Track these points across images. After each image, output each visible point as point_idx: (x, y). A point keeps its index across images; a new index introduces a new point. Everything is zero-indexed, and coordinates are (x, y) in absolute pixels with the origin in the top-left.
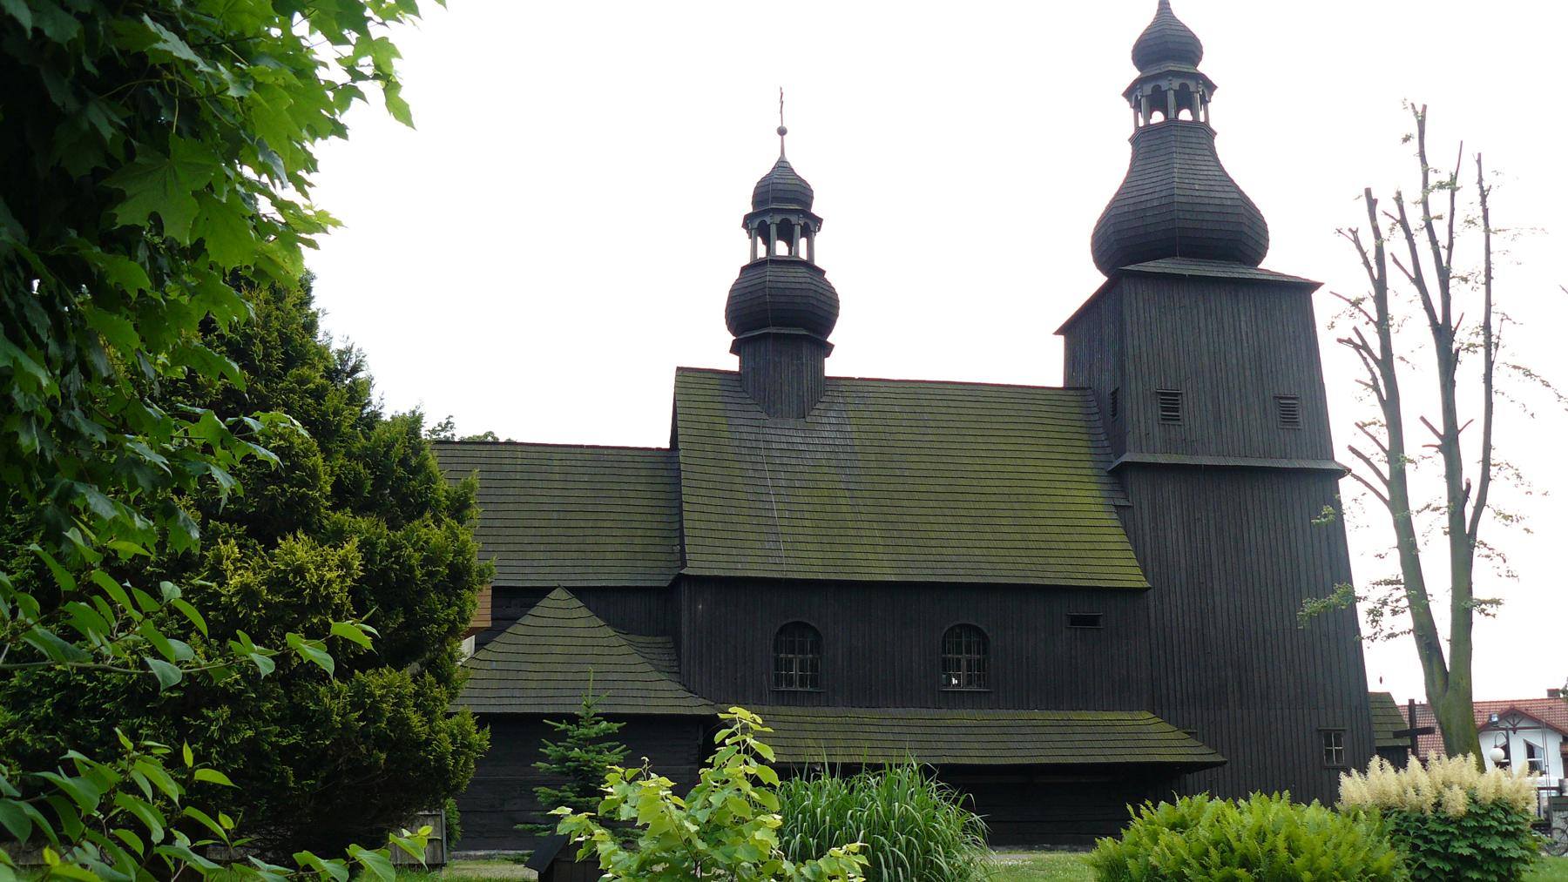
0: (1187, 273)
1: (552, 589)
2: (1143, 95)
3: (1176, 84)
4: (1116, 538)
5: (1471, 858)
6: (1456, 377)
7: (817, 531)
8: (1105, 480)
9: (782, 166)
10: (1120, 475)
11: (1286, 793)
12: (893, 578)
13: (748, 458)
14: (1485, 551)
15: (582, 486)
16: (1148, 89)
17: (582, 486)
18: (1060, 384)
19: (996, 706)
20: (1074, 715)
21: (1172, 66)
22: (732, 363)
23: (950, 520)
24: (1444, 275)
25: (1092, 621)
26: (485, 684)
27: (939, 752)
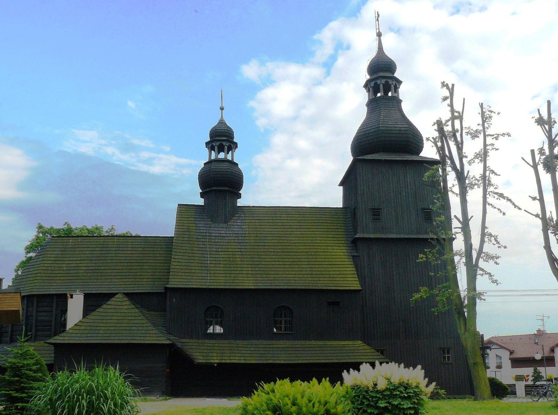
0: (383, 159)
1: (117, 293)
2: (372, 86)
3: (383, 81)
4: (351, 269)
5: (386, 408)
6: (467, 198)
7: (225, 269)
8: (350, 245)
9: (222, 122)
10: (355, 242)
11: (328, 379)
12: (253, 287)
13: (201, 240)
14: (481, 272)
15: (138, 252)
16: (372, 84)
17: (138, 252)
18: (340, 205)
19: (294, 339)
20: (329, 343)
21: (382, 74)
22: (201, 202)
23: (281, 263)
24: (461, 157)
25: (337, 303)
26: (83, 332)
27: (268, 358)
